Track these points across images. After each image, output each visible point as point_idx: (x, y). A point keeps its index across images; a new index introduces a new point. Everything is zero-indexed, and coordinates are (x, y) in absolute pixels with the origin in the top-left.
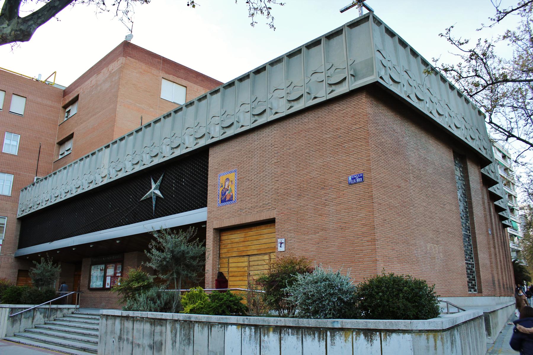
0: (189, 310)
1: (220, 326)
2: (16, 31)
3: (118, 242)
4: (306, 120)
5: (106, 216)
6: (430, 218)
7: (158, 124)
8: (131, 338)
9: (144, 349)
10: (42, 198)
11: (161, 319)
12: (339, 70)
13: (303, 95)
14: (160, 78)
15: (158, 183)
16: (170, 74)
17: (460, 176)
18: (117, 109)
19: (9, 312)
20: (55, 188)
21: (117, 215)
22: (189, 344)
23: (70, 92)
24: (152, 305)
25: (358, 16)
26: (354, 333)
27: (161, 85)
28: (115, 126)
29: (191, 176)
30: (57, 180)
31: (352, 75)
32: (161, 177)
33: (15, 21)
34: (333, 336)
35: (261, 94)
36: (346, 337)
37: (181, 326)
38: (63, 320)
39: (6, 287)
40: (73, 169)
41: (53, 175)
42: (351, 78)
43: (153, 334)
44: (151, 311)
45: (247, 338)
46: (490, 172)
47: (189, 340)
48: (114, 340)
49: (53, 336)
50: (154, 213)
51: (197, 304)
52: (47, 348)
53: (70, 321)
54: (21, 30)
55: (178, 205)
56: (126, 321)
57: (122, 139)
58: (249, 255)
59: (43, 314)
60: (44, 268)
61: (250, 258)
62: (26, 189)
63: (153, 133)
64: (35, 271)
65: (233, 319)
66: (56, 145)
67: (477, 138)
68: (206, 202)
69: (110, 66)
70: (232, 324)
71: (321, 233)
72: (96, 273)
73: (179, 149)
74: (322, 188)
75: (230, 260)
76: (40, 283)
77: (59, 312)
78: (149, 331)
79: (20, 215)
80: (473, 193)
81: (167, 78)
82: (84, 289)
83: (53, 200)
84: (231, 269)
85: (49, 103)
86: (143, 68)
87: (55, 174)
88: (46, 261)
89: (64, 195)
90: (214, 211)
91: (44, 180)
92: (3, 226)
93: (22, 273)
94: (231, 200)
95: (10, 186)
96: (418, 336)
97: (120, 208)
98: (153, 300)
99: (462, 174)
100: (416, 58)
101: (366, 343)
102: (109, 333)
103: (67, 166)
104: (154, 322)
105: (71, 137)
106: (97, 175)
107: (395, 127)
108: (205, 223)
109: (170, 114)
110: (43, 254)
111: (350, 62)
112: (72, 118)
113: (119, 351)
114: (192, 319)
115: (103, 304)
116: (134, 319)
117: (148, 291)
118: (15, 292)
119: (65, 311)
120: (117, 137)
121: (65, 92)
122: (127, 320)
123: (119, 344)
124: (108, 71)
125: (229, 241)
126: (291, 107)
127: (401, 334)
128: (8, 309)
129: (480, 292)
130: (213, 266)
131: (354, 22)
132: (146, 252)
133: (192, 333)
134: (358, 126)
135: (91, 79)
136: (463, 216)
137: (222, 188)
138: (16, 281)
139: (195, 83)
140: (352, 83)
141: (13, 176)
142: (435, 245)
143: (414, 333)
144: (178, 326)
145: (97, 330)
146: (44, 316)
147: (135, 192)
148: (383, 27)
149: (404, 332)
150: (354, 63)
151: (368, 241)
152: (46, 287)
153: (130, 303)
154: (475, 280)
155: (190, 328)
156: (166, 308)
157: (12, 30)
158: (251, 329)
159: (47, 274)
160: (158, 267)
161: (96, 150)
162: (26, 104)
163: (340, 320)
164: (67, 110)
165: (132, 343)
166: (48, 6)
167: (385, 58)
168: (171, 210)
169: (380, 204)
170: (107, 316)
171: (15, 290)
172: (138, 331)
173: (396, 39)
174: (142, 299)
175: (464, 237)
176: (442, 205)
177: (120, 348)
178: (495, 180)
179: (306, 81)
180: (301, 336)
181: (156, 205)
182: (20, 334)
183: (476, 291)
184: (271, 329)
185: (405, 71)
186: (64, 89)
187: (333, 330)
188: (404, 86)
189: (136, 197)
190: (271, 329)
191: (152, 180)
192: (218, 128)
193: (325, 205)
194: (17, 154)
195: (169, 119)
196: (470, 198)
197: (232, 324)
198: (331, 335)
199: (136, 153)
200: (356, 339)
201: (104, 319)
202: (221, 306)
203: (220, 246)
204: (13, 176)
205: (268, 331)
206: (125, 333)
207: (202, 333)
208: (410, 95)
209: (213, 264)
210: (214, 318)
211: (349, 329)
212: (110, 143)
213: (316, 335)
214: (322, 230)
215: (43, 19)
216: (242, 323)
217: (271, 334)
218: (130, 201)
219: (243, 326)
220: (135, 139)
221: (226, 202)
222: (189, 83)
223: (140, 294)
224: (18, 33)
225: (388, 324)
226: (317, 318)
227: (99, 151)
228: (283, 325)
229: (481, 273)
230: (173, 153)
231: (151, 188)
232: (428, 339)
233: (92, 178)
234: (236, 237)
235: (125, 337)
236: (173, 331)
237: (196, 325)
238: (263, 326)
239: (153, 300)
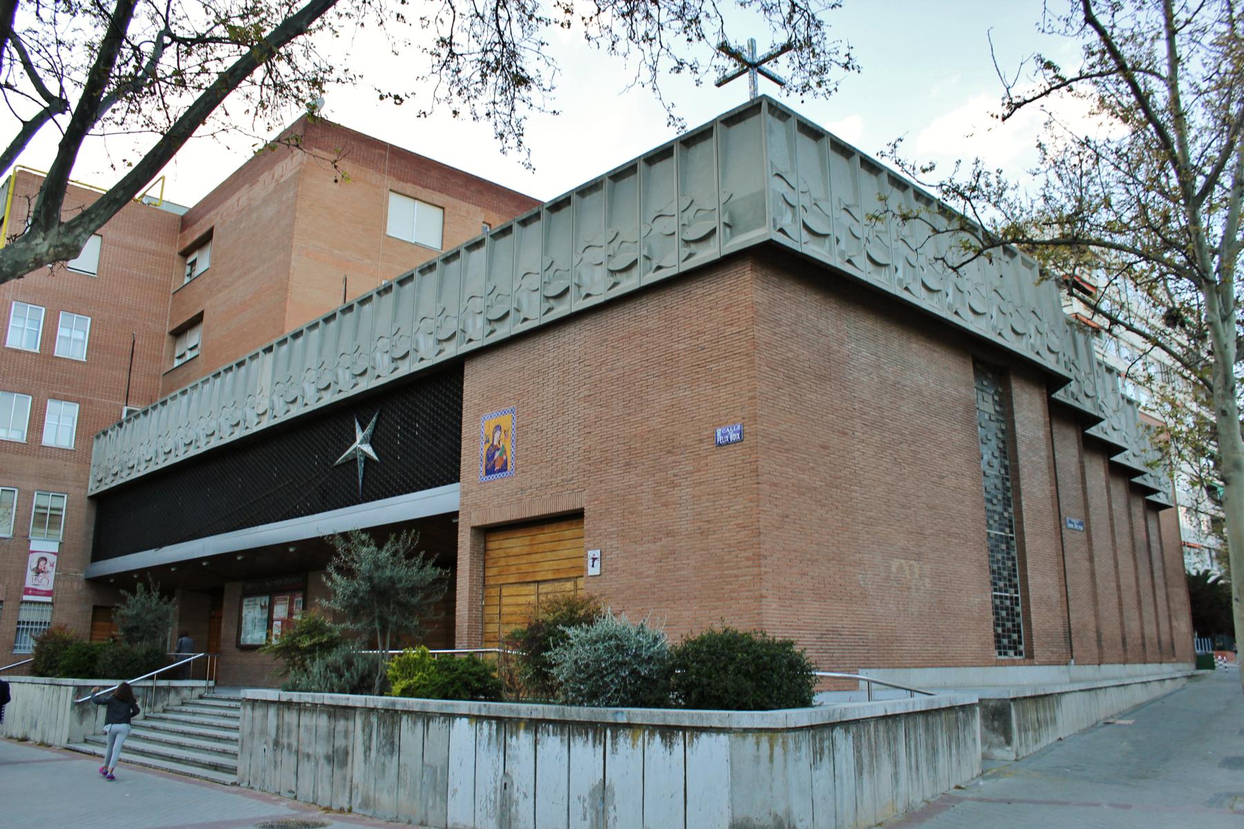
0: (399, 691)
1: (442, 718)
2: (57, 246)
3: (291, 550)
4: (644, 312)
5: (267, 496)
6: (903, 506)
7: (367, 307)
8: (295, 744)
9: (317, 764)
10: (137, 456)
11: (346, 707)
15: (369, 430)
16: (406, 181)
17: (993, 412)
18: (293, 264)
19: (74, 695)
20: (163, 435)
21: (289, 494)
22: (392, 752)
23: (195, 222)
24: (335, 680)
25: (748, 100)
26: (647, 733)
28: (288, 300)
29: (432, 418)
30: (168, 417)
31: (726, 225)
32: (374, 419)
33: (53, 232)
34: (614, 737)
35: (561, 255)
36: (633, 739)
37: (379, 719)
38: (180, 712)
39: (66, 643)
40: (201, 394)
41: (159, 406)
42: (725, 232)
43: (332, 734)
44: (332, 691)
45: (485, 742)
46: (1081, 397)
47: (392, 745)
48: (265, 746)
49: (159, 742)
51: (416, 679)
52: (146, 765)
53: (194, 714)
54: (63, 245)
55: (407, 476)
56: (286, 710)
57: (296, 335)
58: (538, 582)
60: (143, 604)
61: (540, 586)
62: (105, 433)
63: (357, 326)
64: (125, 611)
65: (463, 706)
66: (167, 337)
67: (1033, 331)
68: (459, 470)
69: (276, 168)
70: (462, 716)
71: (665, 541)
72: (252, 613)
73: (407, 361)
74: (669, 452)
75: (503, 591)
76: (135, 635)
77: (172, 695)
78: (326, 730)
79: (93, 489)
80: (1022, 448)
81: (400, 191)
82: (228, 646)
83: (160, 460)
84: (504, 610)
85: (150, 245)
87: (164, 403)
88: (148, 590)
89: (184, 449)
90: (472, 491)
91: (142, 416)
92: (59, 513)
93: (100, 613)
94: (504, 469)
95: (72, 428)
96: (740, 738)
97: (294, 479)
98: (337, 671)
99: (998, 408)
100: (876, 175)
101: (663, 749)
102: (257, 735)
103: (188, 387)
104: (336, 712)
105: (197, 320)
106: (248, 410)
107: (822, 324)
108: (455, 514)
109: (391, 287)
110: (143, 572)
111: (723, 199)
112: (202, 276)
113: (275, 767)
114: (398, 707)
115: (266, 679)
116: (300, 707)
117: (330, 653)
118: (85, 654)
119: (186, 693)
120: (289, 331)
121: (186, 220)
122: (289, 709)
123: (275, 756)
125: (501, 553)
126: (615, 284)
127: (714, 735)
128: (71, 688)
129: (1030, 656)
130: (470, 603)
131: (733, 114)
132: (324, 579)
133: (396, 731)
134: (735, 329)
135: (238, 195)
136: (996, 497)
137: (488, 445)
138: (88, 631)
139: (464, 198)
140: (726, 242)
141: (78, 406)
142: (912, 562)
143: (734, 732)
144: (374, 720)
145: (237, 729)
147: (324, 448)
148: (793, 123)
149: (719, 730)
150: (732, 199)
151: (747, 559)
152: (148, 644)
153: (295, 676)
154: (1019, 632)
155: (393, 724)
156: (362, 686)
157: (50, 246)
158: (491, 725)
159: (149, 617)
160: (345, 607)
161: (247, 357)
162: (101, 249)
163: (626, 710)
164: (190, 260)
165: (297, 752)
166: (105, 199)
167: (793, 188)
168: (394, 488)
169: (775, 485)
170: (254, 702)
171: (85, 650)
172: (308, 729)
173: (826, 143)
174: (317, 668)
175: (997, 540)
176: (934, 479)
177: (276, 762)
178: (1096, 413)
179: (644, 232)
180: (566, 737)
182: (97, 738)
183: (1021, 654)
184: (522, 725)
185: (845, 209)
186: (182, 213)
187: (616, 727)
188: (838, 241)
189: (327, 457)
190: (522, 725)
191: (357, 424)
192: (480, 321)
193: (674, 485)
194: (84, 360)
195: (389, 298)
196: (1015, 459)
197: (462, 716)
198: (612, 736)
199: (324, 366)
200: (649, 743)
201: (249, 708)
202: (452, 683)
203: (485, 561)
204: (78, 406)
205: (518, 728)
206: (285, 734)
207: (413, 732)
208: (853, 259)
209: (470, 598)
210: (434, 704)
211: (639, 726)
212: (274, 341)
213: (590, 736)
214: (667, 535)
215: (98, 222)
216: (476, 713)
217: (522, 733)
218: (315, 466)
219: (478, 719)
220: (323, 335)
221: (494, 473)
222: (449, 198)
223: (313, 660)
224: (60, 249)
225: (695, 718)
226: (594, 706)
227: (252, 358)
228: (540, 717)
229: (1033, 616)
230: (396, 369)
231: (355, 440)
232: (758, 744)
233: (238, 415)
234: (515, 544)
235: (285, 741)
236: (367, 729)
237: (405, 717)
238: (510, 719)
239: (337, 671)
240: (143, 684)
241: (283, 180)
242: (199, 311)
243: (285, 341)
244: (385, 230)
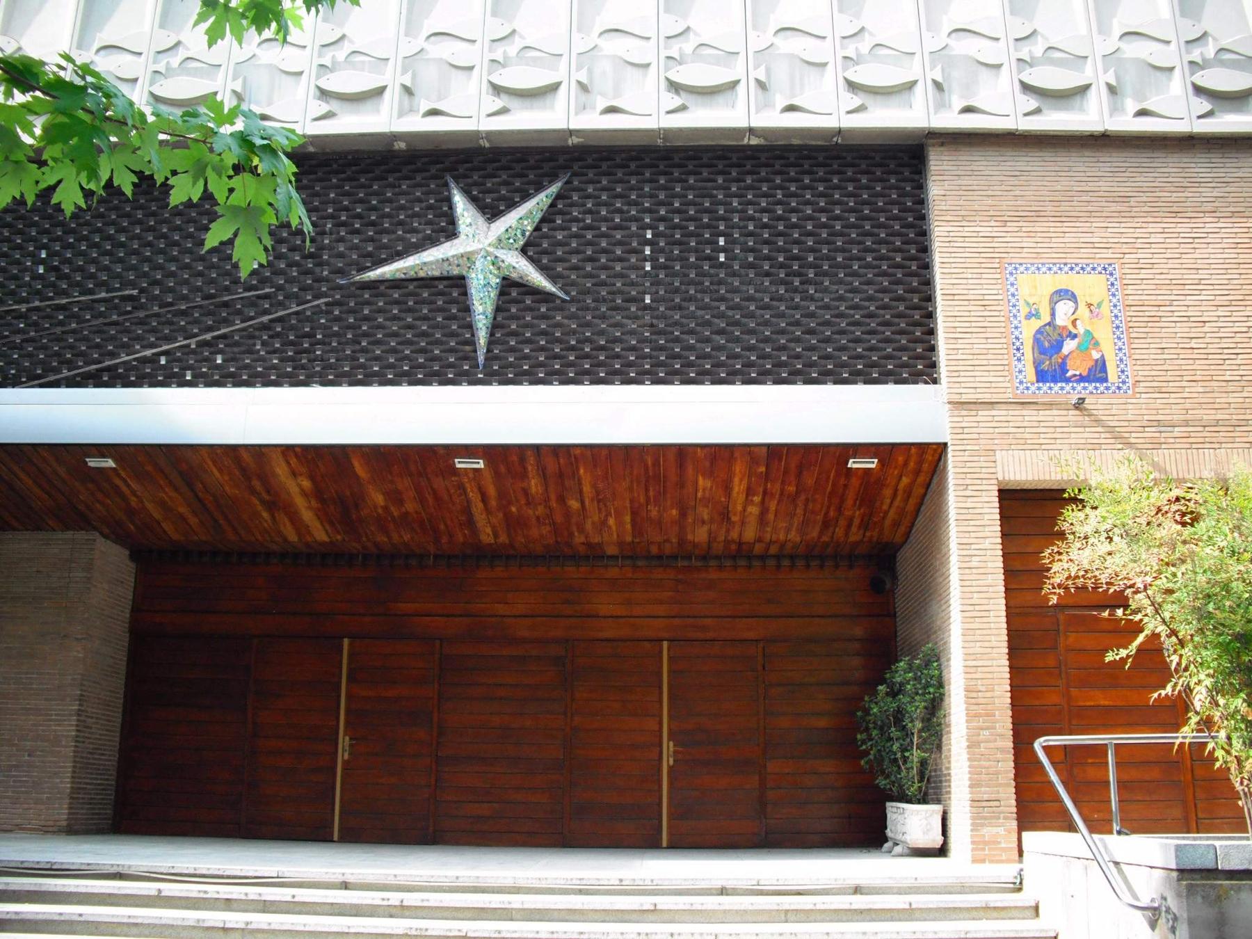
12: (1067, 56)
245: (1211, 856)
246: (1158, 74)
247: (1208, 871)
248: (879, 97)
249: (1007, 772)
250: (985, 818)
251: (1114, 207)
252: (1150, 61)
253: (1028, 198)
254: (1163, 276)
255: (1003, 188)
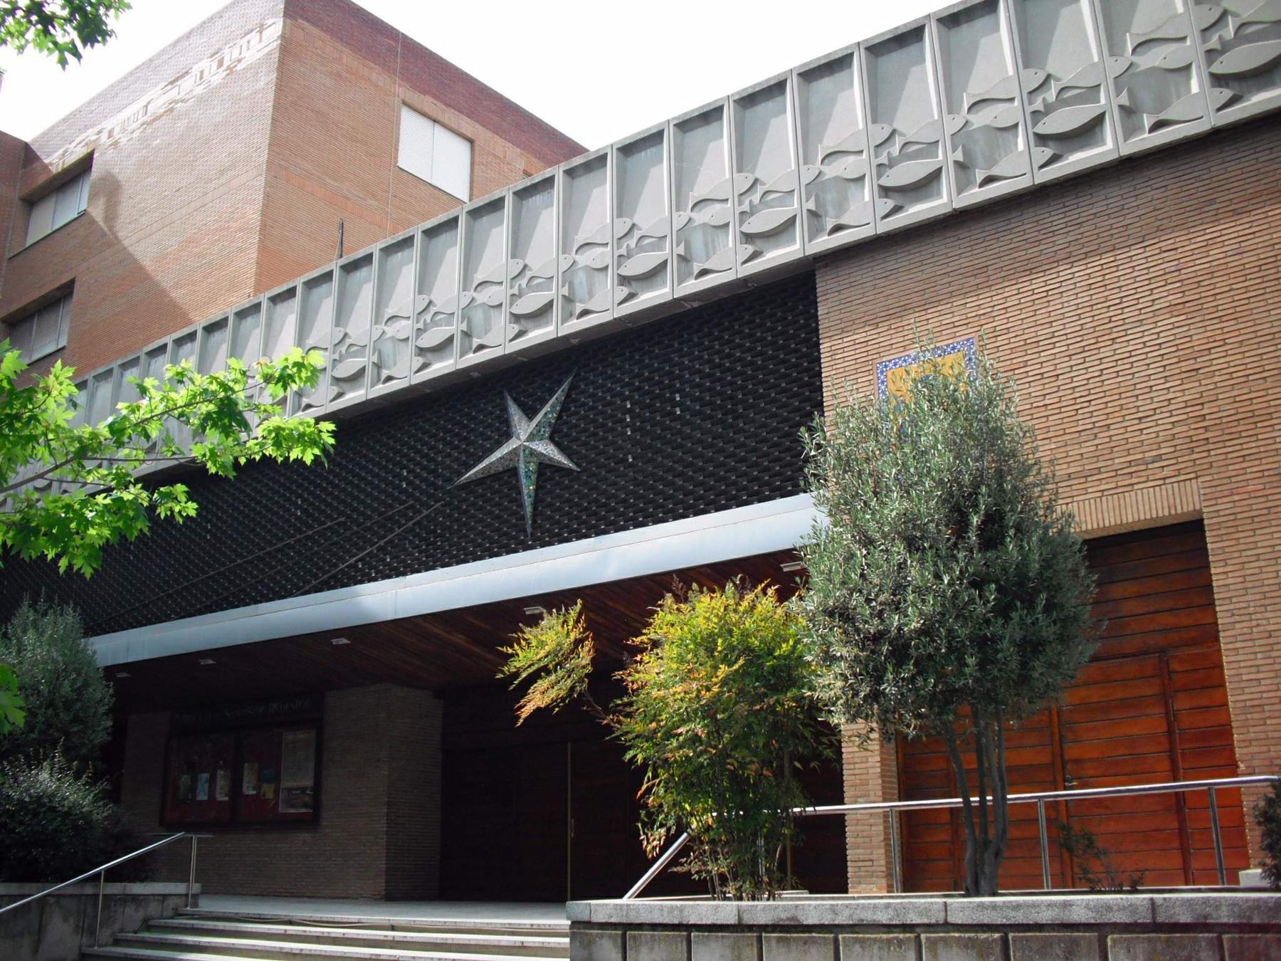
12: (778, 195)
13: (666, 262)
14: (397, 101)
15: (547, 411)
16: (425, 92)
27: (398, 124)
50: (529, 530)
59: (72, 920)
86: (345, 60)
112: (69, 229)
119: (153, 909)
124: (221, 64)
146: (77, 926)
181: (537, 502)
240: (70, 891)
241: (240, 67)
242: (65, 279)
243: (191, 337)
244: (396, 161)
245: (588, 912)
246: (1005, 134)
247: (584, 922)
248: (771, 239)
249: (878, 835)
250: (861, 877)
251: (973, 281)
252: (1165, 67)
253: (897, 295)
254: (1018, 339)
255: (876, 291)
